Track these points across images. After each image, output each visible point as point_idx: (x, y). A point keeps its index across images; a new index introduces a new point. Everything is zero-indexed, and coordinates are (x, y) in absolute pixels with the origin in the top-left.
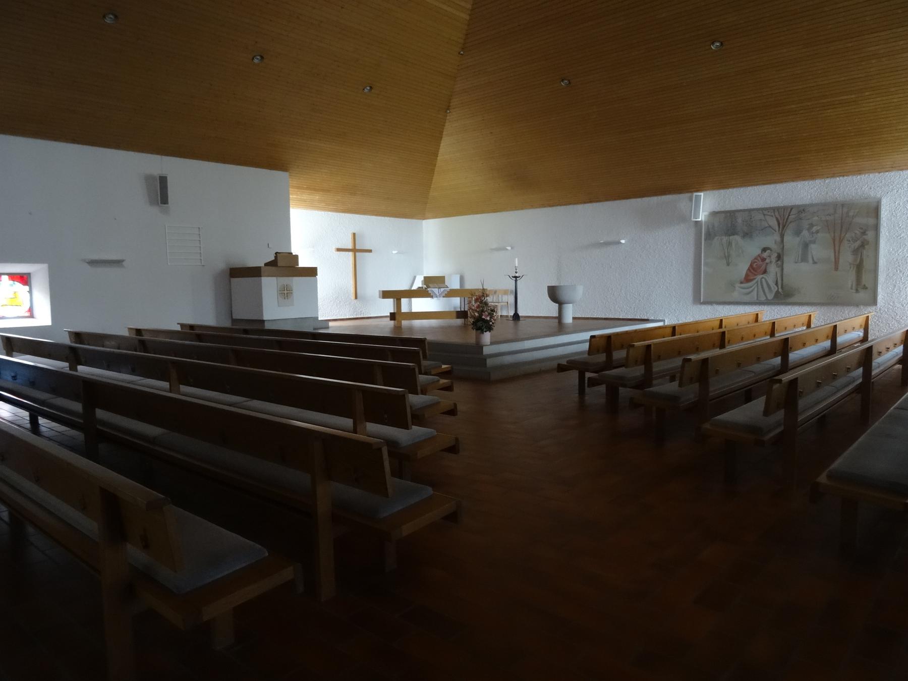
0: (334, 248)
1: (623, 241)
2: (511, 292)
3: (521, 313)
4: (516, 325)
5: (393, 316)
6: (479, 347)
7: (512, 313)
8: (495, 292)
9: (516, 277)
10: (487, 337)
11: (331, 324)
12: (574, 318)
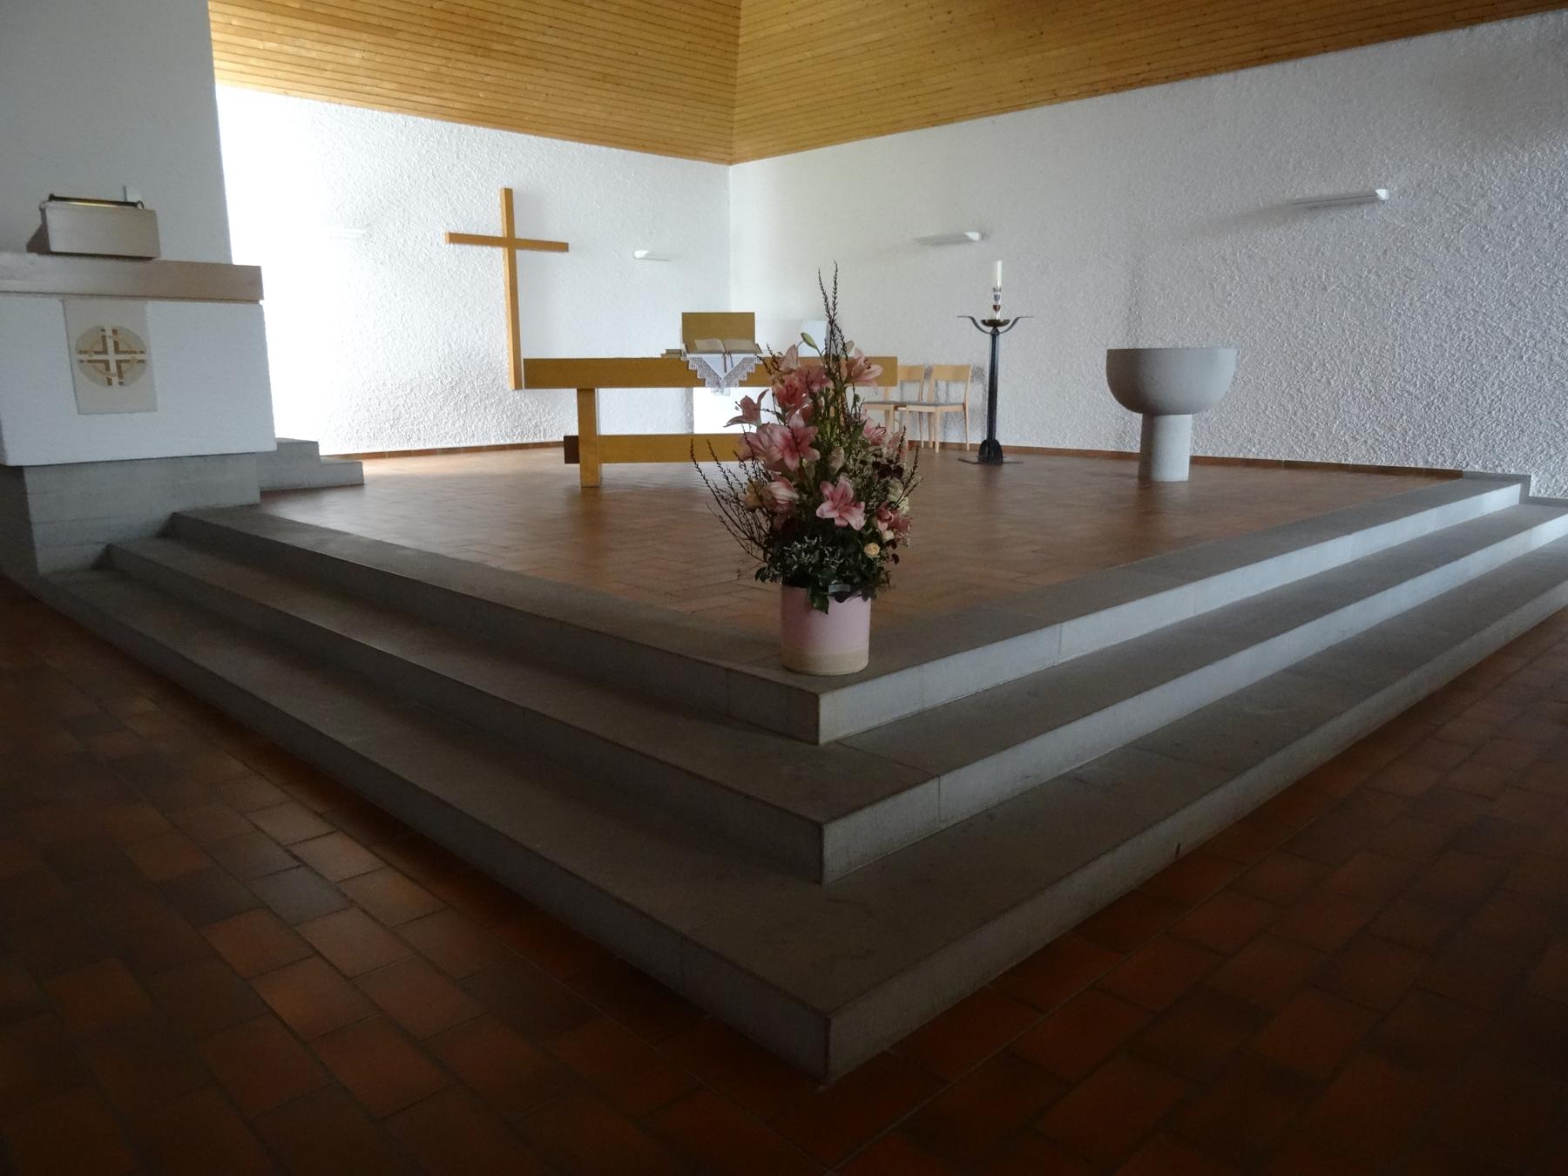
0: (442, 239)
1: (1382, 193)
2: (978, 372)
3: (1004, 438)
4: (989, 483)
5: (572, 448)
6: (796, 696)
7: (977, 437)
8: (928, 373)
9: (994, 324)
10: (848, 628)
11: (369, 469)
12: (1195, 461)
